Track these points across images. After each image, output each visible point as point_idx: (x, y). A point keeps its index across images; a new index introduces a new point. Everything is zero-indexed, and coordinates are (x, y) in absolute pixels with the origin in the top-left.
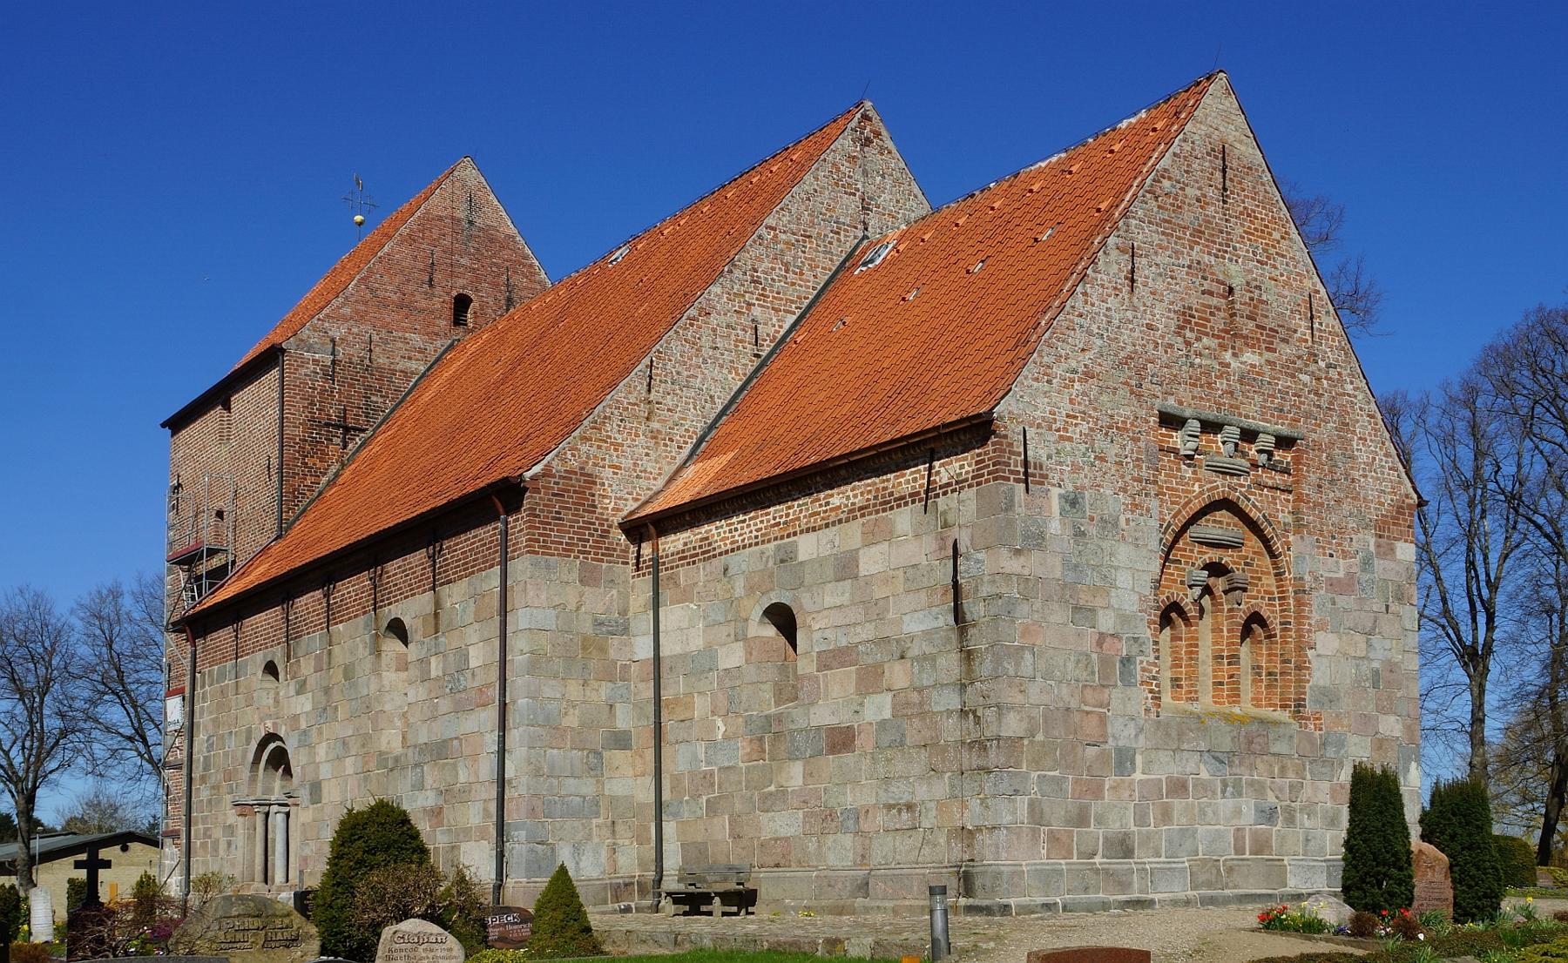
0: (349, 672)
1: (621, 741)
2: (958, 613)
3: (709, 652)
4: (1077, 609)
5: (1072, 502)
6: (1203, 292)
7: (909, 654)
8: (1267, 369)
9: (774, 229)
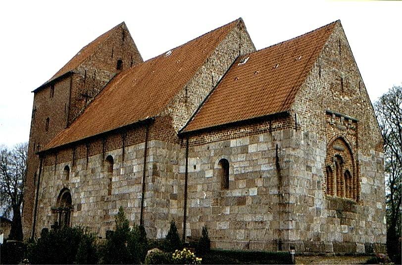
0: (93, 171)
1: (174, 197)
2: (278, 165)
3: (203, 172)
4: (308, 167)
5: (306, 135)
6: (336, 79)
7: (262, 176)
8: (350, 101)
9: (218, 51)
